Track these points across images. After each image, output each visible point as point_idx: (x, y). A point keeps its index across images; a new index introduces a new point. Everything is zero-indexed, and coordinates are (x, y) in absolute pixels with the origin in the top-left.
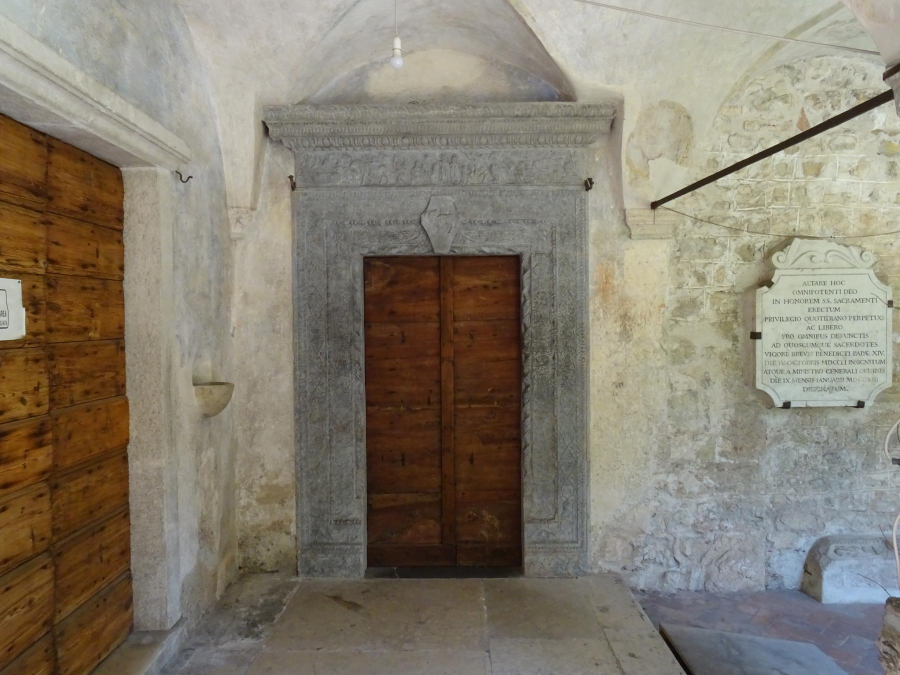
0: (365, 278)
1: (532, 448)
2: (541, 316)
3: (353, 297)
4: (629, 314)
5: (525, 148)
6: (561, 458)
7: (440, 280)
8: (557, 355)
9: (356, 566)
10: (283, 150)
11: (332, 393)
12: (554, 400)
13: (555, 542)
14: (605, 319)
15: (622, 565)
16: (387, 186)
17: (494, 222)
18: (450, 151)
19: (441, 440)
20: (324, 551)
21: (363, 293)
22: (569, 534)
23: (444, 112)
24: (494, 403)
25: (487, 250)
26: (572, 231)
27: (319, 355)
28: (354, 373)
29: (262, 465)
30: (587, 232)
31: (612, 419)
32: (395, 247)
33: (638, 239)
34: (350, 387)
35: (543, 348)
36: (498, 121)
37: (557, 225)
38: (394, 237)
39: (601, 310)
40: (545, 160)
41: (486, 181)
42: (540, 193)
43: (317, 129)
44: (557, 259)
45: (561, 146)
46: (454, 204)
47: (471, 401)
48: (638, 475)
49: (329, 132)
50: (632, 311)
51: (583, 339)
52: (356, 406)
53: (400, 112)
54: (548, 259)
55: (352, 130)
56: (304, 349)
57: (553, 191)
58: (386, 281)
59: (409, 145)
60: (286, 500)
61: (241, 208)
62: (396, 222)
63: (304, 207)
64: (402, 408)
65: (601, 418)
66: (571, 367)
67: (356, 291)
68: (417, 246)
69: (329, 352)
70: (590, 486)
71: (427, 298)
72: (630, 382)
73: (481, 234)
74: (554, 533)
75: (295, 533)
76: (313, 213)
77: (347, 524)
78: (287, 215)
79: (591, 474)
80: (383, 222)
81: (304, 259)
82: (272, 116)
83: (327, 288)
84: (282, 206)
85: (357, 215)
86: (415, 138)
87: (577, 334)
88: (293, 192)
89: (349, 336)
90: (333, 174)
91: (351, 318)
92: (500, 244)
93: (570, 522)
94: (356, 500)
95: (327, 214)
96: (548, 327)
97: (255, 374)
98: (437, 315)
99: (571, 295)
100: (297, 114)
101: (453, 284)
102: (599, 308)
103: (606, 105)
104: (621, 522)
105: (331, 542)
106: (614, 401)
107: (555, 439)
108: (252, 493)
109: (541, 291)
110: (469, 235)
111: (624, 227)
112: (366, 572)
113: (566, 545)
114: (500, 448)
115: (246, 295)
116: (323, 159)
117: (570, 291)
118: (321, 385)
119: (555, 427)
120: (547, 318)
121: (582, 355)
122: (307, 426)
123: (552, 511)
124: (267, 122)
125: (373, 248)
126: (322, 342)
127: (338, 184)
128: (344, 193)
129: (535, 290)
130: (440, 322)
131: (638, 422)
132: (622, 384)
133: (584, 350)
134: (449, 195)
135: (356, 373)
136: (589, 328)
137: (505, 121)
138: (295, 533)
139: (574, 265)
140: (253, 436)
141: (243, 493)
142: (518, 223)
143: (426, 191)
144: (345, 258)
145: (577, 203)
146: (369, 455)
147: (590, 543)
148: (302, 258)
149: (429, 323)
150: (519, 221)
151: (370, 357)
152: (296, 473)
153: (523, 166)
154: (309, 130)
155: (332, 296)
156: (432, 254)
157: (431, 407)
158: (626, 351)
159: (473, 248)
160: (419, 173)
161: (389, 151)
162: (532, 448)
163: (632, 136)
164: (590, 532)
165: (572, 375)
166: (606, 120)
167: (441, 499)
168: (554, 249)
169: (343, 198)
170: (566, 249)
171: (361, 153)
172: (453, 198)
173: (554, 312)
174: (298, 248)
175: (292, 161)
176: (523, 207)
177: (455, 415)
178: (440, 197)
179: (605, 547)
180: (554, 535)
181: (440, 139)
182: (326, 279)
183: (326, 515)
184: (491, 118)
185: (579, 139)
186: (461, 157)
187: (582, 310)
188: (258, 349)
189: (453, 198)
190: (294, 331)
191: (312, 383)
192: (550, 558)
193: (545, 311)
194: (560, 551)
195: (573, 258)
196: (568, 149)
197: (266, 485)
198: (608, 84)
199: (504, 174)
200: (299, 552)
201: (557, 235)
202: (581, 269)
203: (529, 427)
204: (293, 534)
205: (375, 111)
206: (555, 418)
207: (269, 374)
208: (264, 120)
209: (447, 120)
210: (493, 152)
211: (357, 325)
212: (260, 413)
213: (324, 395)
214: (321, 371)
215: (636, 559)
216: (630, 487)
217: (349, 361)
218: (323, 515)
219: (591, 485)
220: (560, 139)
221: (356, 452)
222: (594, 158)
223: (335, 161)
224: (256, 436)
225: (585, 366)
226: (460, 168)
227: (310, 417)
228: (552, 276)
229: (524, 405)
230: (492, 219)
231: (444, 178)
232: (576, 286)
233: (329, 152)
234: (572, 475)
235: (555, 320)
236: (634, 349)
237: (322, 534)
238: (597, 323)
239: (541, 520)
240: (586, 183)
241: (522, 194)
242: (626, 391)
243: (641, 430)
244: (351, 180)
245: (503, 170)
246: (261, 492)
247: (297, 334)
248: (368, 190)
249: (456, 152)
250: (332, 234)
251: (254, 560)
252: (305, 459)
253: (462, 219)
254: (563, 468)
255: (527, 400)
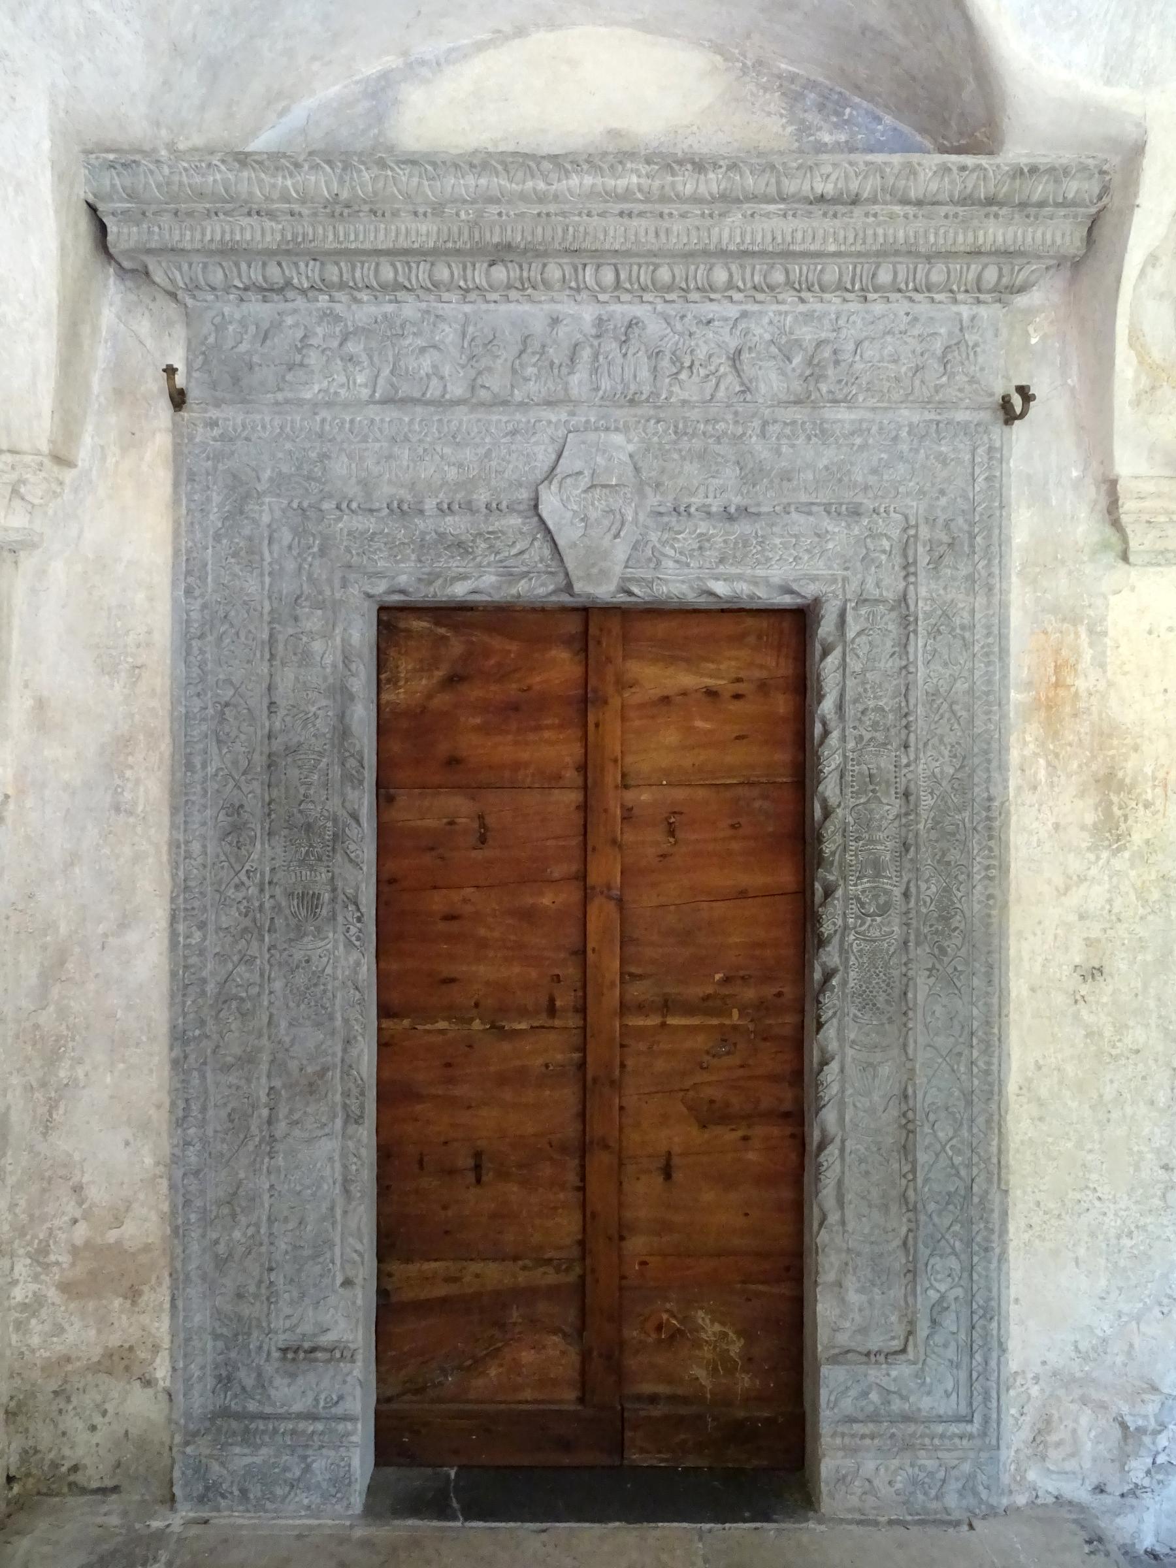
0: (381, 664)
1: (842, 1150)
2: (870, 776)
3: (342, 716)
4: (1120, 774)
5: (833, 303)
6: (926, 1180)
7: (587, 672)
8: (918, 887)
9: (341, 1482)
10: (154, 299)
11: (278, 985)
12: (905, 1014)
13: (906, 1418)
14: (1052, 785)
15: (1094, 1480)
16: (443, 404)
17: (744, 511)
18: (624, 310)
19: (582, 1115)
20: (248, 1438)
21: (374, 707)
22: (948, 1395)
23: (611, 183)
24: (730, 1015)
25: (721, 588)
26: (965, 537)
27: (244, 878)
28: (340, 929)
29: (78, 1189)
30: (1004, 542)
31: (1070, 1069)
32: (463, 577)
33: (1150, 564)
34: (329, 970)
35: (878, 868)
36: (767, 215)
37: (921, 521)
38: (461, 547)
39: (1042, 762)
40: (889, 338)
41: (721, 394)
42: (874, 429)
43: (247, 230)
44: (921, 616)
45: (937, 297)
46: (631, 456)
47: (667, 1006)
48: (1143, 1228)
49: (279, 238)
50: (1129, 765)
51: (992, 843)
52: (346, 1021)
53: (483, 181)
54: (894, 615)
55: (346, 235)
56: (200, 860)
57: (910, 425)
58: (439, 674)
59: (509, 287)
60: (146, 1288)
61: (25, 453)
62: (469, 507)
63: (208, 458)
64: (477, 1025)
65: (1039, 1068)
66: (955, 922)
67: (352, 698)
68: (525, 575)
69: (273, 870)
70: (1007, 1260)
71: (549, 722)
72: (1123, 966)
73: (707, 545)
74: (904, 1393)
75: (168, 1383)
76: (235, 476)
77: (316, 1360)
78: (161, 480)
79: (1012, 1228)
80: (430, 505)
81: (204, 606)
82: (113, 186)
83: (269, 688)
84: (148, 456)
85: (359, 482)
86: (525, 266)
87: (975, 829)
88: (178, 418)
89: (330, 824)
90: (291, 367)
91: (336, 772)
92: (760, 572)
93: (951, 1361)
94: (341, 1290)
95: (271, 479)
96: (891, 806)
97: (63, 929)
98: (578, 769)
99: (958, 720)
100: (185, 179)
101: (623, 684)
102: (1036, 755)
103: (1084, 168)
104: (1095, 1360)
105: (268, 1410)
106: (1076, 1017)
107: (908, 1127)
108: (47, 1266)
109: (871, 704)
110: (673, 547)
111: (1109, 531)
112: (372, 1491)
113: (940, 1429)
114: (745, 1138)
115: (41, 705)
116: (265, 325)
117: (956, 707)
118: (249, 961)
119: (910, 1091)
120: (887, 782)
121: (986, 888)
122: (203, 1077)
123: (900, 1330)
124: (101, 207)
125: (403, 579)
126: (253, 840)
127: (308, 396)
128: (323, 421)
129: (855, 701)
130: (585, 788)
131: (1144, 1078)
132: (1100, 970)
133: (993, 872)
134: (617, 429)
135: (348, 930)
136: (1008, 813)
137: (785, 216)
138: (168, 1383)
139: (967, 635)
140: (53, 1105)
141: (22, 1268)
142: (810, 513)
143: (554, 419)
144: (321, 605)
145: (978, 459)
146: (385, 1154)
147: (1008, 1422)
148: (200, 601)
149: (556, 791)
150: (815, 509)
151: (392, 881)
152: (174, 1213)
153: (827, 353)
154: (223, 233)
155: (282, 712)
156: (565, 599)
157: (557, 1023)
158: (1111, 877)
159: (683, 582)
160: (535, 370)
161: (453, 307)
162: (842, 1150)
163: (1152, 259)
164: (1008, 1390)
165: (958, 942)
166: (1075, 217)
167: (582, 1277)
168: (911, 587)
169: (320, 436)
170: (945, 588)
171: (373, 309)
172: (629, 441)
173: (907, 765)
174: (189, 573)
175: (180, 331)
176: (827, 468)
177: (622, 1046)
178: (592, 436)
179: (1049, 1433)
180: (904, 1398)
181: (598, 266)
182: (266, 664)
183: (255, 1334)
184: (745, 206)
185: (991, 275)
186: (654, 328)
187: (989, 761)
188: (73, 859)
189: (629, 441)
190: (174, 810)
191: (222, 957)
192: (895, 1463)
193: (885, 762)
194: (923, 1447)
195: (965, 614)
196: (955, 308)
197: (88, 1244)
198: (1108, 82)
199: (773, 376)
200: (178, 1439)
201: (920, 549)
202: (989, 645)
203: (835, 1089)
204: (161, 1383)
205: (411, 176)
206: (909, 1065)
207: (101, 929)
208: (91, 199)
209: (619, 207)
210: (744, 315)
211: (352, 795)
212: (73, 1040)
213: (254, 991)
214: (247, 922)
215: (1133, 1464)
216: (1122, 1263)
217: (326, 897)
218: (249, 1334)
219: (1012, 1254)
220: (937, 276)
221: (344, 1155)
222: (1027, 335)
223: (300, 334)
224: (62, 1105)
225: (995, 920)
226: (649, 358)
227: (214, 1052)
228: (904, 663)
229: (820, 1026)
230: (737, 500)
231: (605, 384)
232: (971, 691)
233: (282, 306)
234: (957, 1227)
235: (912, 785)
236: (1133, 873)
237: (243, 1388)
238: (1029, 797)
239: (868, 1354)
240: (1006, 403)
241: (823, 433)
242: (1110, 989)
243: (1152, 1103)
244: (342, 386)
245: (772, 363)
246: (73, 1264)
247: (180, 818)
248: (391, 413)
249: (638, 310)
250: (286, 536)
251: (51, 1456)
252: (196, 1173)
253: (653, 500)
254: (932, 1206)
255: (830, 1013)
